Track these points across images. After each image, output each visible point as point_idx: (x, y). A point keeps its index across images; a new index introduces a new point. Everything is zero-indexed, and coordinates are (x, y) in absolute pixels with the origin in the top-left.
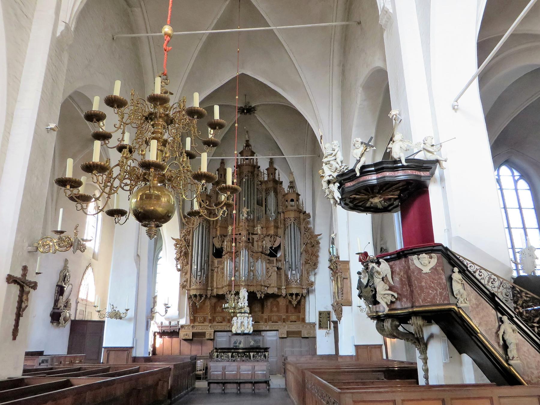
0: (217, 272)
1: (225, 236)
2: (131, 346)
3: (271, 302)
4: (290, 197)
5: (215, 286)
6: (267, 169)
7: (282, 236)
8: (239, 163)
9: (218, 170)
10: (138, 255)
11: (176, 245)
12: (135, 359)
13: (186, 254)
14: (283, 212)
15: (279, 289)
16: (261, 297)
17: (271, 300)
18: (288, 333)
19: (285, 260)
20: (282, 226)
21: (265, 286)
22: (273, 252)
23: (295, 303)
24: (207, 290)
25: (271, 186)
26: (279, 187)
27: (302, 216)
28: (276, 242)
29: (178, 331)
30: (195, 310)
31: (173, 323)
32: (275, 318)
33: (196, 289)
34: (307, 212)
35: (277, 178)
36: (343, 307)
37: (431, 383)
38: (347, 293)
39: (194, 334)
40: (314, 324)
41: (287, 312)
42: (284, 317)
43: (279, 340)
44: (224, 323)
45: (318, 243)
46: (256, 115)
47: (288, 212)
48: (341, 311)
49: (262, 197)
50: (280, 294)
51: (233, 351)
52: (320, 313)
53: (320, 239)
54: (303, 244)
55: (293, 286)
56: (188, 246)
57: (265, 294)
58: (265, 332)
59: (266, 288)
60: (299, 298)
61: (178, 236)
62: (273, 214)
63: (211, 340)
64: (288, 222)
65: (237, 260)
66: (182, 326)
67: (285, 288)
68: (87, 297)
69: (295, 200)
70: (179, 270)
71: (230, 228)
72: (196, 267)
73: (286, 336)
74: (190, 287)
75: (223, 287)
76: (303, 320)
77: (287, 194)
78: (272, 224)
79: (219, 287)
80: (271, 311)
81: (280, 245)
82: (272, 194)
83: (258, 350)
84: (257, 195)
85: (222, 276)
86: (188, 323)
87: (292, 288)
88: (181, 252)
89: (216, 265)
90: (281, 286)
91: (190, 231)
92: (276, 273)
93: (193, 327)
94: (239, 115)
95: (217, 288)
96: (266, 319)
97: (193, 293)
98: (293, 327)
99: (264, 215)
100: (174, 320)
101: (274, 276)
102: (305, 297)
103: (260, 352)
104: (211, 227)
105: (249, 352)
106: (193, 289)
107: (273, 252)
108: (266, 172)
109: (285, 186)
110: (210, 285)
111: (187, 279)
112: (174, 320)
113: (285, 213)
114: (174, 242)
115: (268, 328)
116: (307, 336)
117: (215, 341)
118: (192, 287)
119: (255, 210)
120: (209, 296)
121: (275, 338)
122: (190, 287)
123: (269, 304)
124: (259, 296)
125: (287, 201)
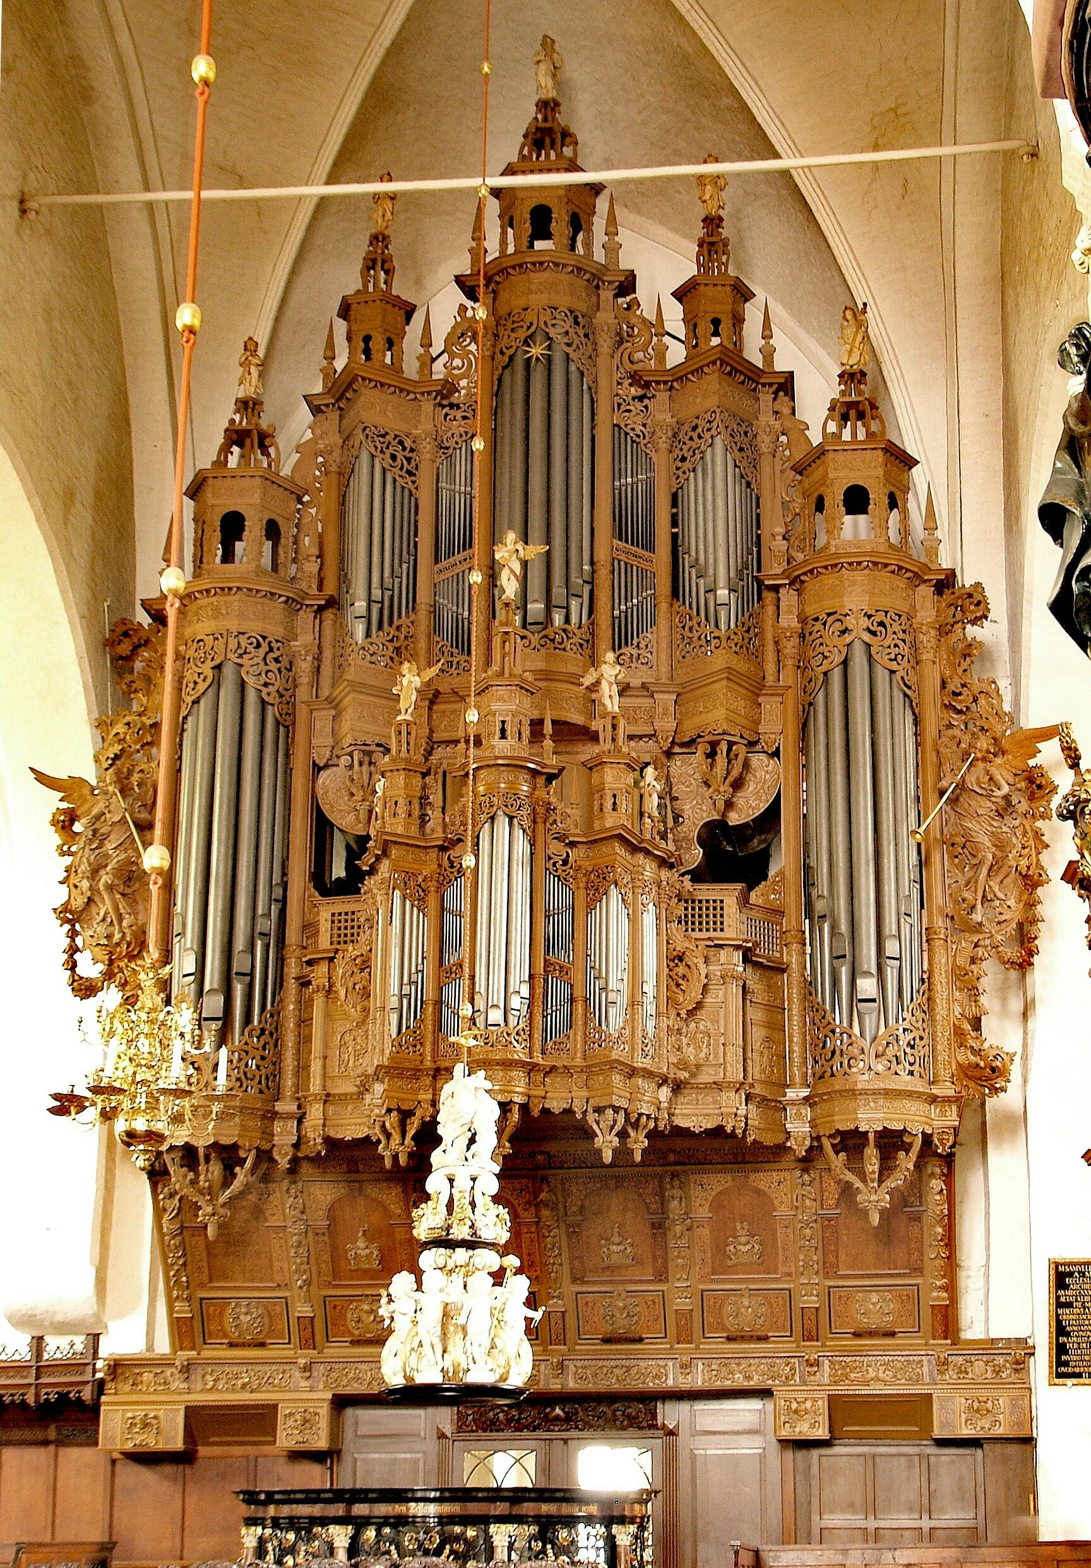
0: (330, 991)
3: (717, 1205)
4: (841, 476)
5: (315, 1086)
6: (680, 295)
14: (796, 582)
16: (623, 1152)
17: (717, 1182)
20: (788, 677)
22: (734, 855)
23: (875, 1198)
24: (272, 1116)
25: (712, 402)
26: (766, 419)
28: (751, 787)
29: (87, 1394)
30: (200, 1261)
31: (57, 1346)
32: (747, 1311)
35: (753, 355)
37: (221, 1015)
39: (200, 1422)
40: (1019, 1353)
41: (829, 1269)
49: (650, 484)
50: (769, 1140)
54: (932, 797)
55: (863, 1081)
57: (653, 1135)
58: (684, 1407)
59: (665, 1093)
62: (722, 593)
66: (117, 1367)
69: (877, 496)
75: (364, 1089)
76: (947, 1321)
77: (820, 453)
80: (721, 1261)
81: (772, 814)
82: (719, 456)
84: (616, 473)
86: (163, 1345)
87: (853, 1093)
92: (735, 990)
93: (187, 1369)
95: (327, 1098)
96: (685, 1316)
98: (880, 1375)
99: (664, 606)
100: (63, 1328)
105: (484, 1521)
108: (674, 316)
110: (288, 1082)
112: (63, 1328)
114: (53, 801)
115: (698, 1379)
116: (966, 1432)
119: (603, 574)
120: (283, 1162)
121: (749, 1447)
123: (702, 1212)
124: (606, 1144)
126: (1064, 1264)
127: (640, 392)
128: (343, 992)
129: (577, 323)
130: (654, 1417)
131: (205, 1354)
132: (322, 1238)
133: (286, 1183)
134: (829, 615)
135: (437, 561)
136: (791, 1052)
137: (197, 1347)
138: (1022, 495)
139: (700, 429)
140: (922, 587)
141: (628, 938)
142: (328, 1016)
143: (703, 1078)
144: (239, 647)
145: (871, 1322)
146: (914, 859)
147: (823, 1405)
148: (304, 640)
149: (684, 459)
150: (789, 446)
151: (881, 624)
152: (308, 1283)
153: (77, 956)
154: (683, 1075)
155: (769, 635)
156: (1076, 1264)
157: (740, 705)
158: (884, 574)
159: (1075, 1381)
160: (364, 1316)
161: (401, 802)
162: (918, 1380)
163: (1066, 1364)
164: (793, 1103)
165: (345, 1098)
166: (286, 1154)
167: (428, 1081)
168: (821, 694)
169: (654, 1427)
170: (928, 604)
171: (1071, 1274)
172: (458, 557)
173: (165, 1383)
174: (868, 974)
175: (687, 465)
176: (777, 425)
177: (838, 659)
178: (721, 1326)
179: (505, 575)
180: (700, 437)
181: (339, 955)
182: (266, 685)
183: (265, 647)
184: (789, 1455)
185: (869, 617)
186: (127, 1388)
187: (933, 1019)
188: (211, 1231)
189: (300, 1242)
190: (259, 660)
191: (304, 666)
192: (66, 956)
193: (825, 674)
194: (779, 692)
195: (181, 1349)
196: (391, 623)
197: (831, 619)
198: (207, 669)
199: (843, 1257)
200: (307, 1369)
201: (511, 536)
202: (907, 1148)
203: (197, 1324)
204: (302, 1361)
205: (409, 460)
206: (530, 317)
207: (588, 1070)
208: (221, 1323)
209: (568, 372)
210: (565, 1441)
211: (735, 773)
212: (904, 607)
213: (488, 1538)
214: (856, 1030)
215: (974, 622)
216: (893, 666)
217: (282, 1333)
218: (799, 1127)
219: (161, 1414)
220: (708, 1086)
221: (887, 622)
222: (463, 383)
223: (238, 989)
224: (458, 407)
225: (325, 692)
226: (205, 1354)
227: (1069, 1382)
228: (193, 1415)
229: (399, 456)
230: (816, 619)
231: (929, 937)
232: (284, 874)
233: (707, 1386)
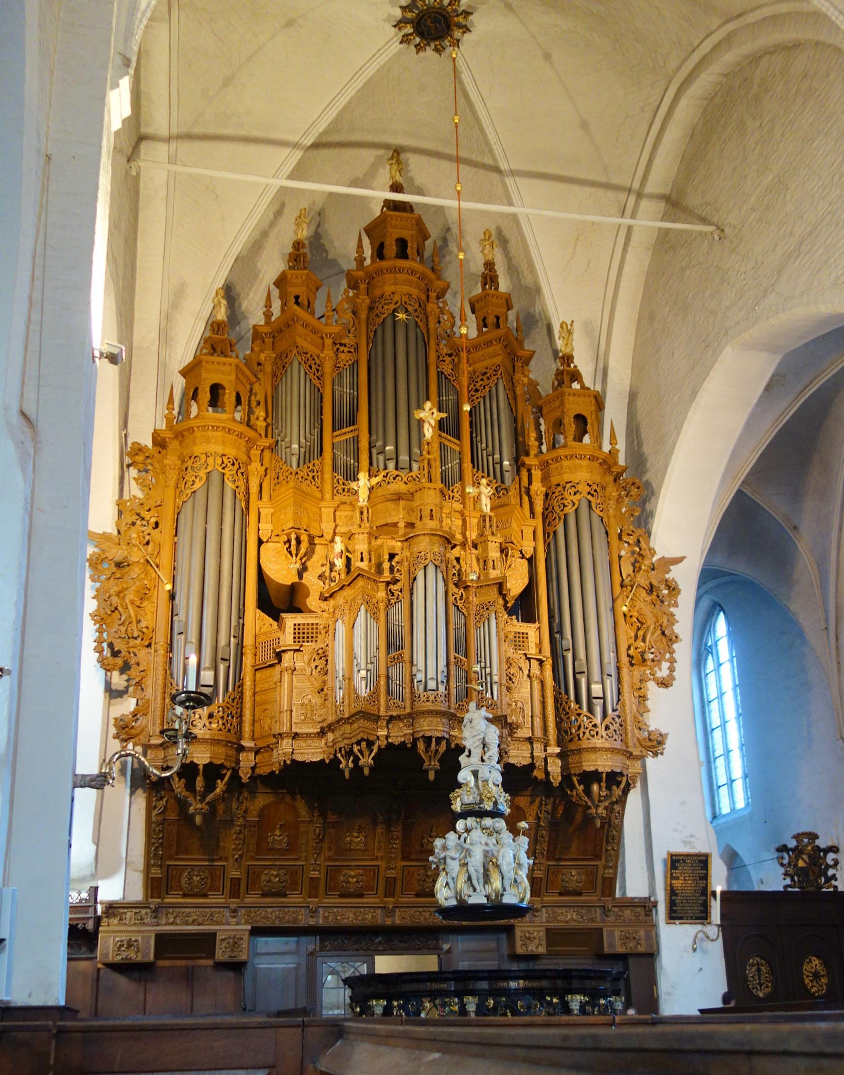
10: (23, 414)
29: (90, 926)
32: (352, 877)
40: (646, 906)
44: (294, 899)
51: (484, 985)
52: (675, 861)
55: (598, 742)
66: (112, 908)
67: (559, 755)
68: (296, 146)
73: (542, 950)
76: (609, 885)
86: (137, 894)
93: (156, 912)
116: (620, 949)
117: (248, 973)
126: (676, 855)
129: (420, 306)
132: (252, 829)
134: (567, 483)
135: (334, 430)
137: (241, 895)
139: (488, 375)
144: (223, 462)
145: (572, 886)
147: (542, 934)
149: (477, 390)
151: (595, 491)
156: (681, 855)
159: (680, 921)
160: (273, 878)
162: (593, 920)
163: (675, 912)
166: (248, 773)
171: (678, 861)
173: (141, 919)
179: (426, 426)
180: (488, 378)
183: (237, 466)
189: (240, 831)
190: (234, 472)
192: (96, 644)
195: (152, 897)
197: (568, 486)
203: (164, 882)
205: (318, 370)
206: (396, 298)
208: (179, 882)
209: (417, 333)
217: (219, 887)
219: (140, 939)
221: (598, 490)
223: (222, 667)
224: (345, 345)
227: (677, 922)
228: (160, 938)
230: (558, 485)
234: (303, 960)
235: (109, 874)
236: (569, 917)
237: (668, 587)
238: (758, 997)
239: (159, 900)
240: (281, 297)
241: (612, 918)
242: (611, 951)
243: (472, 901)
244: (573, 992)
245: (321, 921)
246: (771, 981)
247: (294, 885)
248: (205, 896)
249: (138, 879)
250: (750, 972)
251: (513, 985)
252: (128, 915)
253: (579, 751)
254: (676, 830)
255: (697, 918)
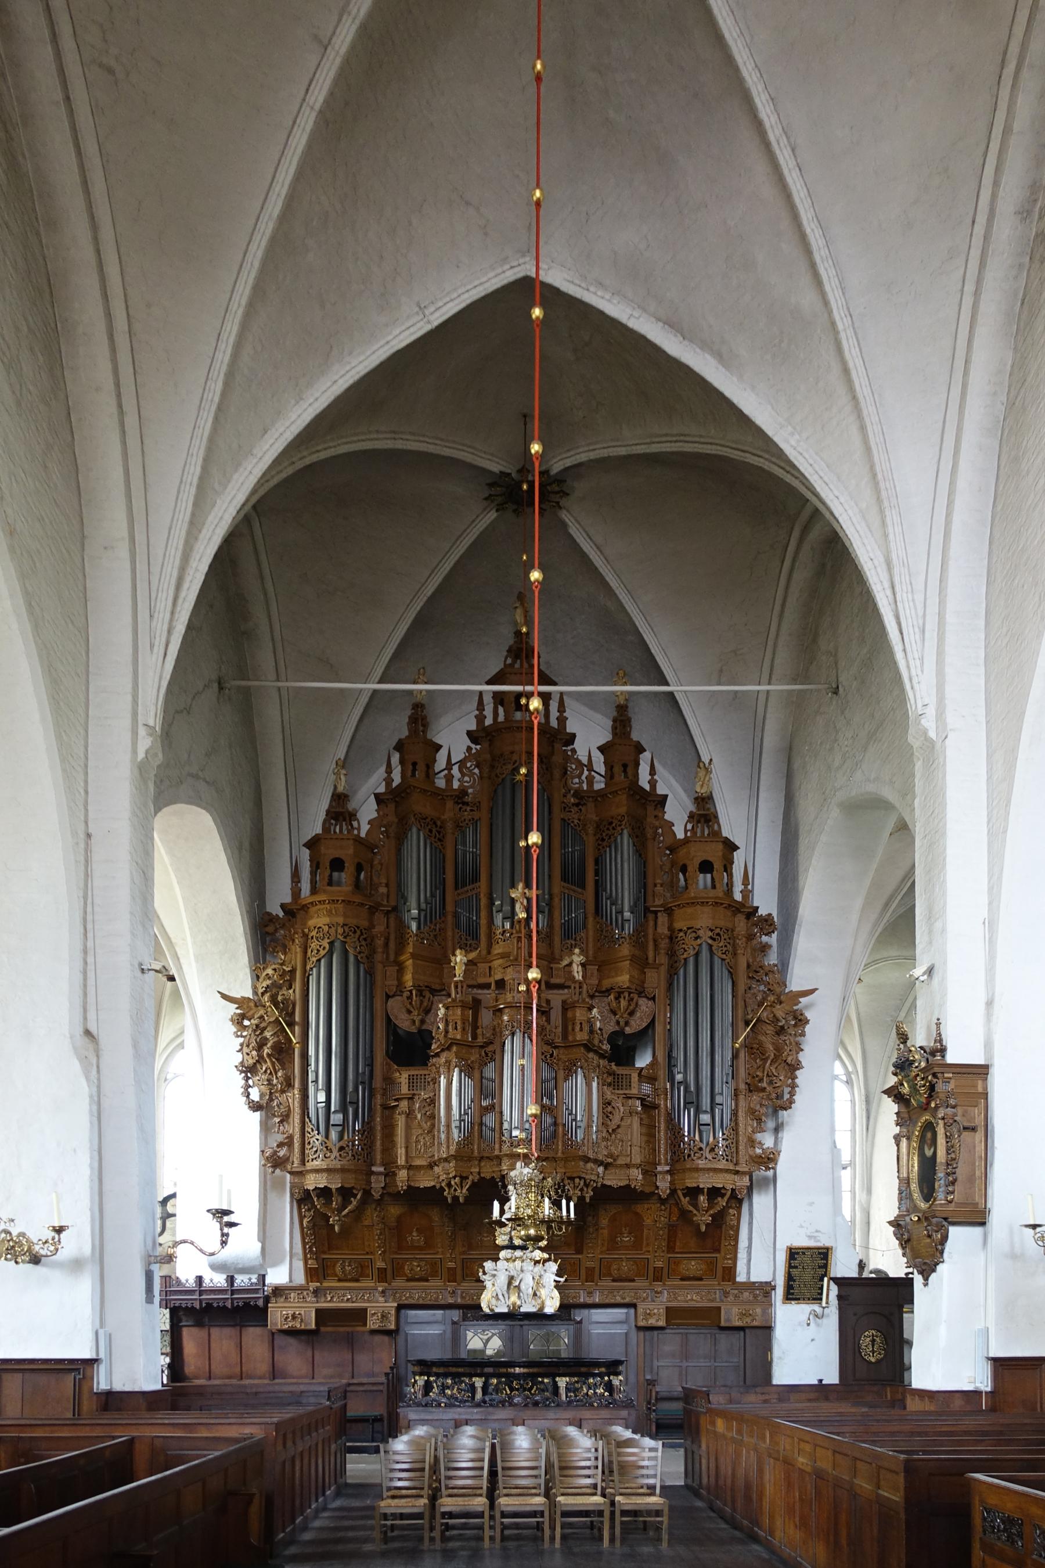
0: (410, 1115)
1: (434, 992)
2: (87, 1354)
5: (401, 1161)
6: (601, 749)
7: (660, 993)
8: (489, 721)
9: (399, 747)
10: (88, 1033)
11: (238, 1021)
12: (112, 1401)
13: (282, 1052)
14: (669, 911)
15: (649, 1172)
17: (613, 1209)
18: (672, 1313)
19: (671, 1078)
20: (663, 959)
21: (600, 1163)
23: (704, 1219)
26: (650, 819)
27: (741, 925)
29: (260, 1303)
31: (242, 1280)
33: (328, 1170)
34: (762, 912)
36: (953, 1231)
38: (971, 1179)
40: (766, 1289)
41: (671, 1249)
42: (659, 1264)
43: (634, 1333)
44: (435, 1283)
45: (801, 1021)
46: (564, 515)
47: (689, 910)
48: (945, 1238)
50: (647, 1190)
51: (490, 1370)
52: (793, 1253)
53: (808, 1006)
54: (741, 1024)
56: (291, 1025)
58: (585, 1312)
59: (601, 1169)
60: (722, 1202)
61: (244, 989)
62: (627, 915)
63: (388, 1333)
64: (690, 945)
65: (490, 1071)
66: (278, 1291)
69: (718, 865)
70: (255, 1107)
71: (459, 958)
72: (322, 1097)
73: (662, 1323)
74: (303, 1162)
75: (431, 1166)
76: (730, 1273)
78: (625, 950)
79: (418, 1162)
82: (626, 841)
83: (583, 1370)
84: (564, 846)
85: (426, 1126)
86: (300, 1279)
88: (260, 1047)
89: (404, 1089)
90: (655, 1164)
91: (293, 972)
93: (316, 1292)
94: (493, 515)
95: (410, 1168)
96: (590, 1272)
97: (312, 1182)
98: (691, 1297)
99: (591, 920)
100: (244, 1271)
101: (635, 1129)
102: (740, 1202)
103: (594, 1375)
104: (379, 957)
105: (553, 1376)
106: (317, 1171)
107: (622, 1050)
108: (599, 764)
109: (677, 815)
111: (291, 1138)
112: (244, 1271)
113: (678, 913)
114: (232, 1009)
116: (738, 1323)
117: (401, 1339)
118: (310, 1165)
119: (556, 900)
121: (621, 1330)
122: (303, 1162)
123: (604, 1222)
125: (684, 869)
127: (577, 801)
128: (419, 1116)
130: (570, 1315)
131: (325, 1284)
133: (374, 1206)
135: (456, 888)
136: (659, 1147)
138: (801, 869)
140: (739, 915)
141: (582, 1095)
142: (408, 1128)
143: (619, 1162)
146: (730, 1056)
148: (379, 928)
149: (603, 840)
150: (662, 834)
152: (384, 1252)
153: (250, 1090)
154: (610, 1160)
155: (651, 937)
157: (636, 973)
158: (721, 909)
161: (459, 1023)
164: (660, 1173)
165: (419, 1168)
167: (476, 1163)
168: (682, 972)
169: (570, 1320)
170: (742, 924)
171: (798, 1253)
172: (469, 887)
174: (706, 1112)
175: (605, 843)
176: (657, 823)
177: (692, 952)
178: (610, 1275)
181: (417, 1097)
182: (360, 953)
183: (358, 932)
184: (641, 1334)
185: (712, 930)
186: (282, 1300)
187: (737, 1134)
188: (336, 1228)
191: (379, 942)
193: (685, 959)
194: (657, 967)
196: (431, 922)
198: (325, 943)
199: (678, 1244)
200: (383, 1292)
201: (521, 886)
202: (723, 1196)
203: (321, 1271)
204: (380, 1289)
205: (439, 833)
207: (566, 1160)
208: (334, 1270)
210: (521, 1326)
211: (631, 1008)
212: (730, 926)
213: (555, 1384)
214: (697, 1137)
215: (766, 935)
216: (724, 956)
218: (664, 1184)
220: (621, 1166)
222: (470, 791)
225: (392, 957)
226: (325, 1284)
229: (434, 830)
230: (681, 930)
231: (736, 1094)
232: (372, 1051)
233: (602, 1302)
234: (449, 1328)
235: (275, 1264)
236: (689, 1297)
237: (795, 1018)
238: (870, 1362)
239: (318, 1284)
240: (402, 762)
241: (731, 1298)
242: (727, 1325)
243: (497, 1310)
244: (560, 1375)
245: (459, 1300)
246: (884, 1350)
247: (434, 1273)
248: (357, 1281)
249: (299, 1265)
250: (865, 1341)
251: (517, 1370)
252: (292, 1295)
253: (355, 1171)
254: (801, 1227)
255: (814, 1299)
